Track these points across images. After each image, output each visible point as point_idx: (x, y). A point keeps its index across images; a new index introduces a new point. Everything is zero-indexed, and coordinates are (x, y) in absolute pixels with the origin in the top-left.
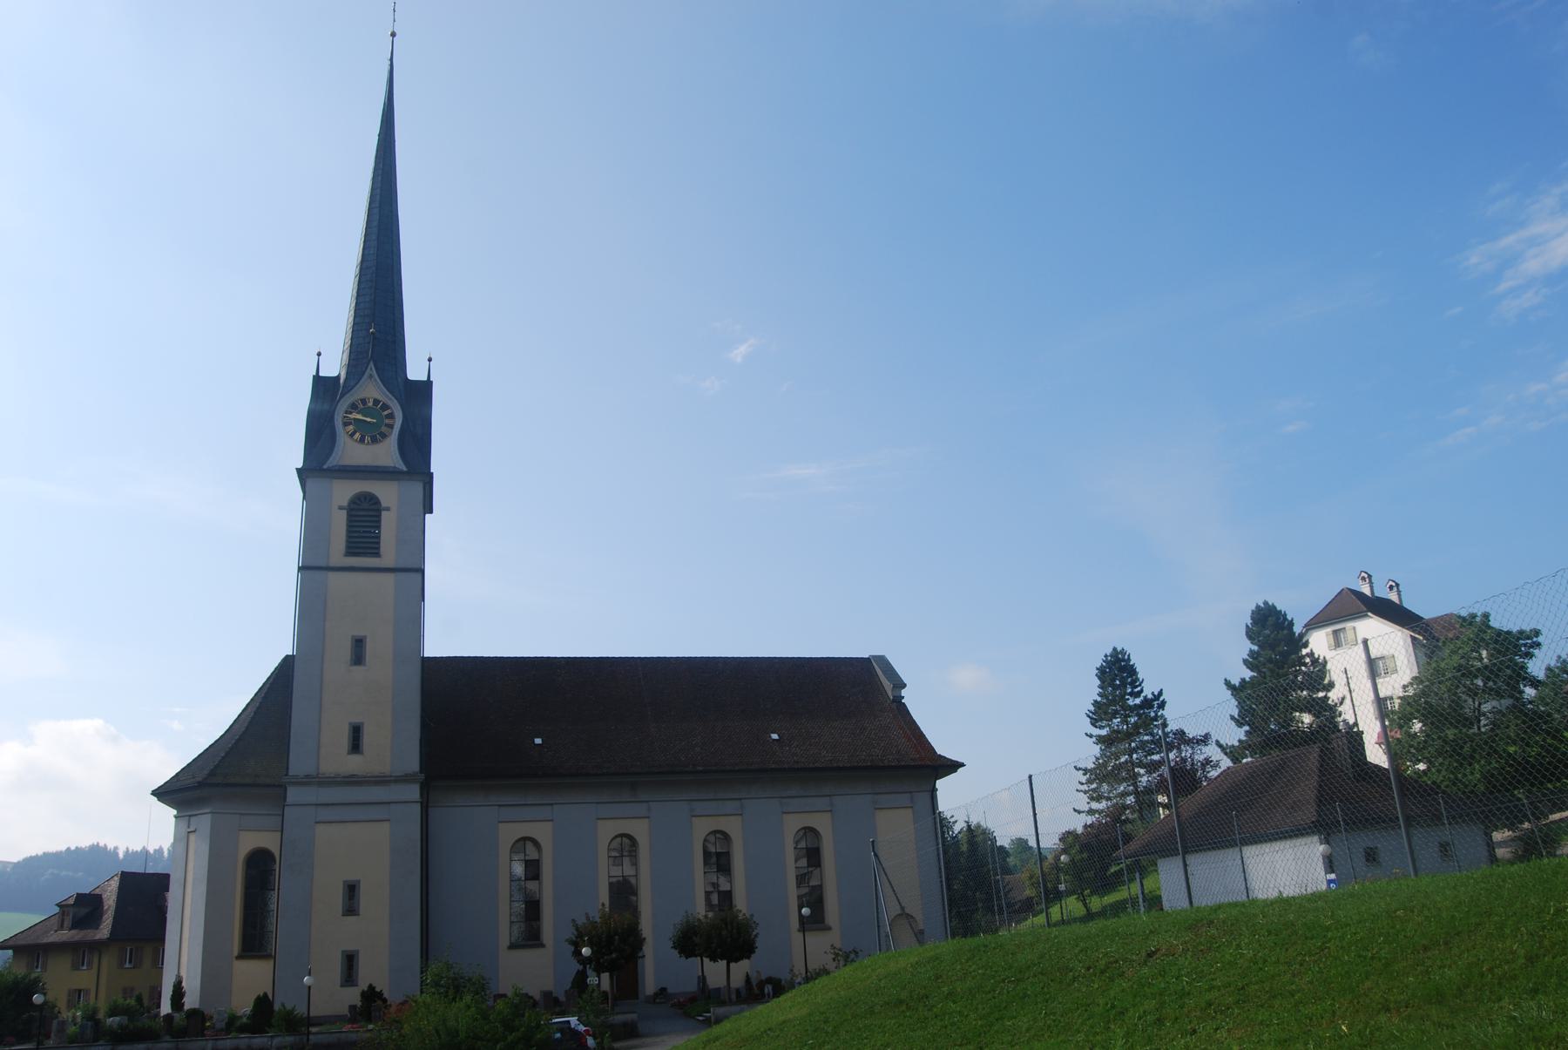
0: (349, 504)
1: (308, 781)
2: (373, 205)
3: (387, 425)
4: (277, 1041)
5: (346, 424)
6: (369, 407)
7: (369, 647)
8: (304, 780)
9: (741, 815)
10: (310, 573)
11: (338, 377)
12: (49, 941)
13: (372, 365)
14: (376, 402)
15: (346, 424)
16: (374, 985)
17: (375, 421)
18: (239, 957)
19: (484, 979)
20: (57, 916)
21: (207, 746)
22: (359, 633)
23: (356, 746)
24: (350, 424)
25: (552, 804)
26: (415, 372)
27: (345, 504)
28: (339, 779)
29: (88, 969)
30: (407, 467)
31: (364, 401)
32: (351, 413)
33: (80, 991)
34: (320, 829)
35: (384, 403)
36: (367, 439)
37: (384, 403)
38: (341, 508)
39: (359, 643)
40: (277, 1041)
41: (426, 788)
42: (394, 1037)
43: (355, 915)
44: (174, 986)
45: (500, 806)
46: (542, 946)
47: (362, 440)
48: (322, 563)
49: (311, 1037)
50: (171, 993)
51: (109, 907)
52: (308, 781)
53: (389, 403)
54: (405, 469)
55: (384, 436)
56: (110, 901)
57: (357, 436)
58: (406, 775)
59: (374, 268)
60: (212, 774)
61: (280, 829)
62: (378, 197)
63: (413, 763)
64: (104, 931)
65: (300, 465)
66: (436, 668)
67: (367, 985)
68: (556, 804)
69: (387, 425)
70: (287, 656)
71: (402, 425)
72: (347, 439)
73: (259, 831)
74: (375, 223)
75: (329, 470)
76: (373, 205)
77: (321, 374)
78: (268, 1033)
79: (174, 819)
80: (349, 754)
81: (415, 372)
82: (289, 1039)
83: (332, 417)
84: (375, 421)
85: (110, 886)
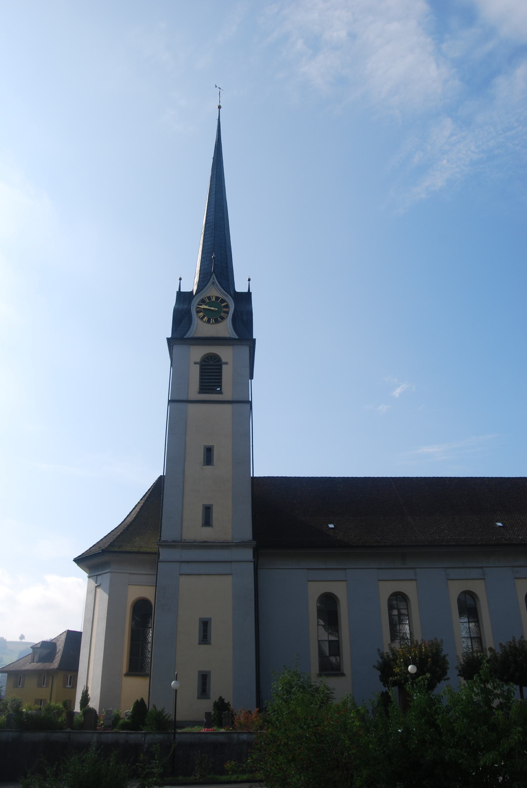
0: (201, 362)
1: (173, 545)
2: (212, 194)
3: (224, 312)
4: (149, 737)
5: (198, 312)
6: (213, 302)
7: (215, 452)
8: (172, 544)
9: (484, 579)
10: (175, 405)
11: (192, 292)
12: (25, 669)
13: (214, 276)
14: (217, 298)
15: (198, 312)
16: (223, 698)
17: (217, 309)
18: (127, 675)
19: (328, 689)
20: (31, 654)
21: (110, 531)
22: (209, 444)
23: (207, 521)
24: (201, 312)
25: (345, 569)
26: (240, 287)
27: (198, 360)
28: (196, 544)
29: (46, 687)
30: (238, 336)
31: (209, 298)
32: (201, 305)
33: (41, 700)
34: (183, 579)
35: (222, 299)
36: (212, 321)
37: (222, 299)
38: (196, 363)
39: (209, 451)
40: (149, 737)
41: (256, 554)
42: (314, 737)
43: (208, 644)
44: (83, 693)
45: (308, 569)
46: (343, 675)
47: (209, 321)
48: (184, 398)
49: (177, 736)
50: (81, 698)
51: (60, 650)
52: (173, 545)
53: (226, 299)
54: (237, 337)
55: (223, 319)
56: (60, 647)
57: (206, 319)
58: (243, 542)
59: (213, 226)
60: (112, 545)
61: (155, 585)
62: (214, 189)
63: (247, 533)
64: (55, 664)
65: (170, 336)
66: (255, 480)
67: (218, 697)
68: (348, 568)
69: (224, 312)
70: (161, 476)
71: (234, 312)
72: (200, 322)
73: (139, 585)
74: (213, 203)
75: (188, 339)
76: (212, 194)
77: (181, 291)
78: (142, 730)
79: (88, 578)
80: (202, 526)
81: (240, 287)
82: (159, 737)
83: (190, 310)
84: (217, 309)
85: (61, 638)
